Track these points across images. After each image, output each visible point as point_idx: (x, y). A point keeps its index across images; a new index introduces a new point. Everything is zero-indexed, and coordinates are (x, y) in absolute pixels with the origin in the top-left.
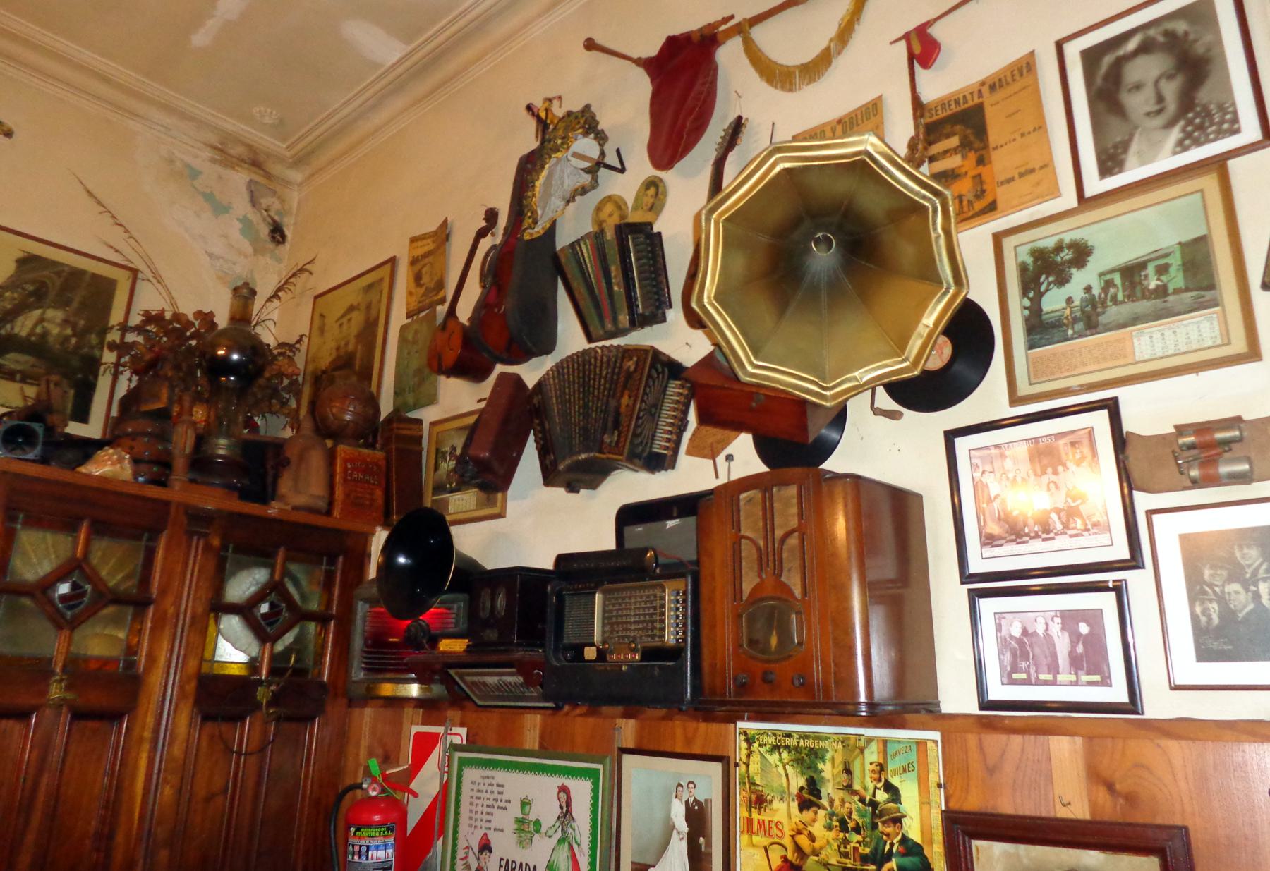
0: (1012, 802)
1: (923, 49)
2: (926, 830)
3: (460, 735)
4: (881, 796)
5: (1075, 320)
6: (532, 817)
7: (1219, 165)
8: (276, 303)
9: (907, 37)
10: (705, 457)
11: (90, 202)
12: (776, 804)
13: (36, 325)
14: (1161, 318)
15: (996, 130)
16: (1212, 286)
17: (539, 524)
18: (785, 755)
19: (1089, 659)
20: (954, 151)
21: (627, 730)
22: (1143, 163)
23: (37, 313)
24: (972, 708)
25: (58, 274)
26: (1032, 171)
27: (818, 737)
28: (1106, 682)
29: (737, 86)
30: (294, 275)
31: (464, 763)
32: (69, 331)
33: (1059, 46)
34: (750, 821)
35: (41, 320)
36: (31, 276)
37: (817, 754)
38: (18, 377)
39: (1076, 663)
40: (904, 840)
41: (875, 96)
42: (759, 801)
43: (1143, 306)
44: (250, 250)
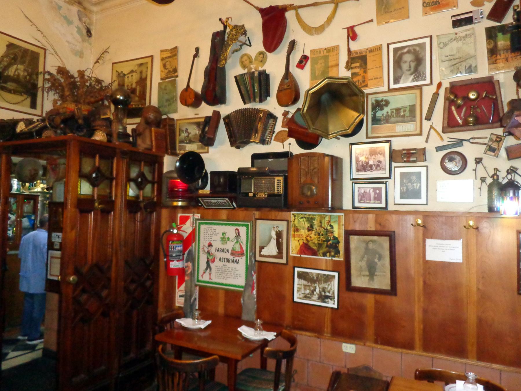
0: (358, 227)
1: (352, 35)
2: (339, 234)
3: (198, 216)
4: (329, 228)
5: (384, 120)
6: (226, 237)
7: (420, 87)
8: (97, 64)
9: (348, 28)
10: (280, 142)
11: (27, 20)
12: (301, 230)
13: (15, 71)
14: (402, 122)
15: (370, 64)
16: (415, 117)
17: (224, 157)
18: (304, 219)
19: (378, 198)
20: (358, 67)
21: (257, 214)
22: (404, 82)
23: (15, 66)
24: (350, 208)
25: (20, 50)
26: (378, 78)
27: (313, 215)
28: (381, 203)
29: (293, 30)
30: (103, 53)
31: (200, 224)
32: (26, 74)
33: (388, 45)
34: (294, 235)
35: (17, 69)
36: (11, 51)
37: (313, 219)
38: (12, 92)
39: (375, 199)
40: (334, 237)
41: (336, 44)
42: (297, 230)
43: (400, 119)
44: (80, 40)
